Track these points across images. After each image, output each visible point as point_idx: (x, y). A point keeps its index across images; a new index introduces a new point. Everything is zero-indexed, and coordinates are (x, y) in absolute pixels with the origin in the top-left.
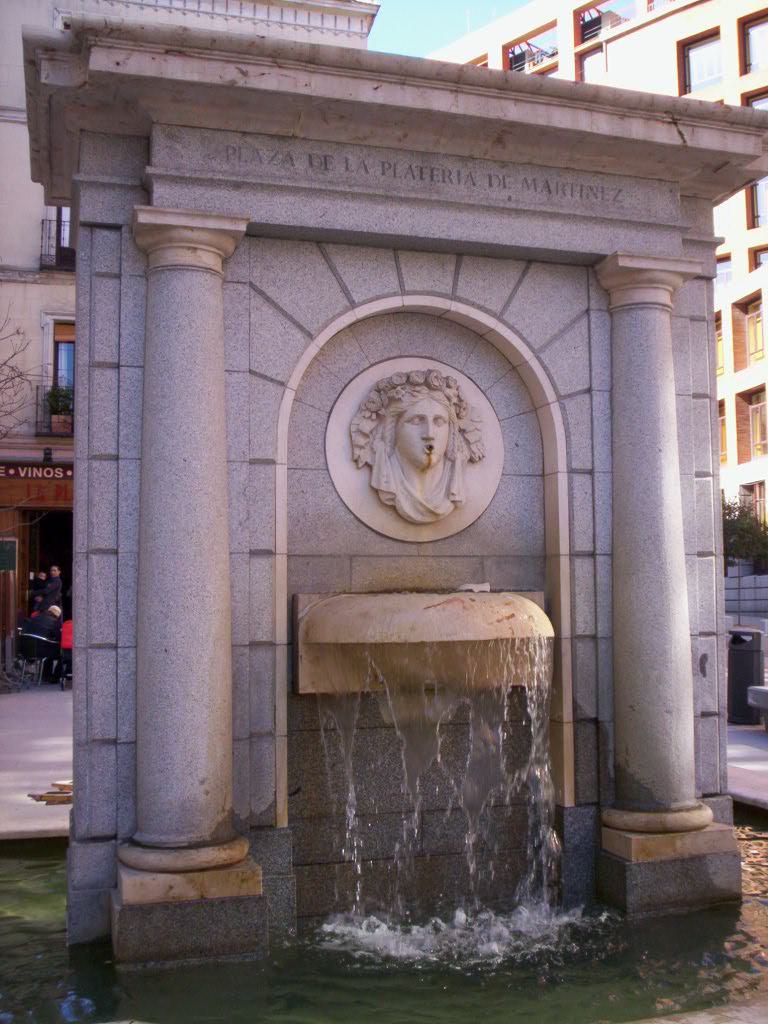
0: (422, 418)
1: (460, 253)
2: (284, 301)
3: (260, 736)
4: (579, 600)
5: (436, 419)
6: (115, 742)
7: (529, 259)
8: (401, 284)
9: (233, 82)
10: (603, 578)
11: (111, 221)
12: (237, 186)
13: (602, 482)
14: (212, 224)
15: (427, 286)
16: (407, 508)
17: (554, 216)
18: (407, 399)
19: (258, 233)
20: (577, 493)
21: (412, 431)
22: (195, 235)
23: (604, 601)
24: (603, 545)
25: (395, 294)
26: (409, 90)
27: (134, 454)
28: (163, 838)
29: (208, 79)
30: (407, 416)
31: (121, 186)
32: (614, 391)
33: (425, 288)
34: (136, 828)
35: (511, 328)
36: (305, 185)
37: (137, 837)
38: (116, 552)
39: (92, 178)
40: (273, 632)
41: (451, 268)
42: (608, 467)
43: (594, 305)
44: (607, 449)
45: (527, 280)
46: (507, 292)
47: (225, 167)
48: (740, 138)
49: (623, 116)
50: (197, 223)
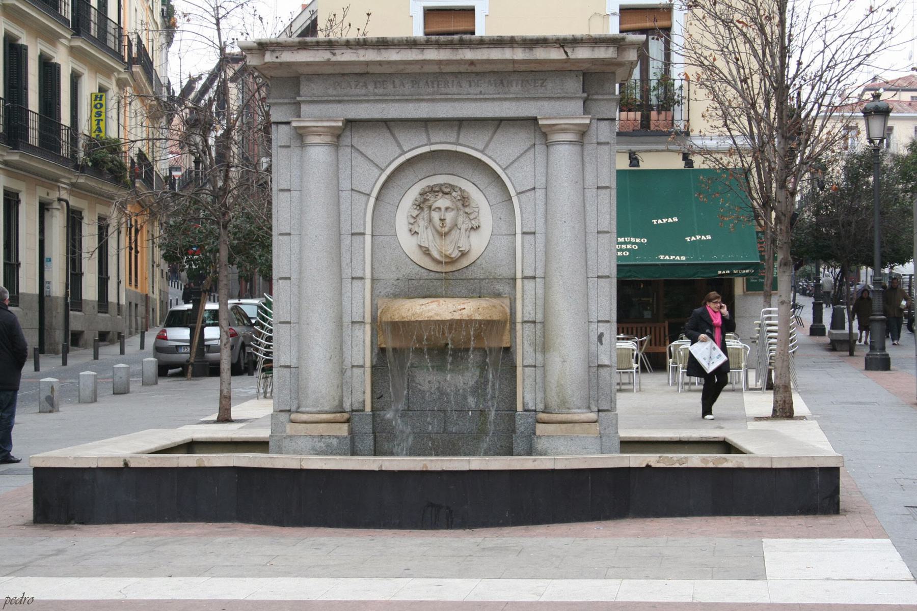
0: (440, 209)
1: (460, 124)
2: (369, 153)
3: (460, 350)
4: (527, 301)
5: (447, 209)
6: (534, 322)
7: (499, 123)
8: (429, 139)
9: (329, 60)
10: (540, 292)
11: (285, 120)
12: (340, 102)
13: (540, 238)
14: (325, 124)
15: (443, 140)
16: (436, 254)
17: (506, 99)
18: (432, 199)
19: (351, 124)
20: (527, 246)
21: (436, 216)
22: (319, 129)
23: (540, 303)
24: (540, 273)
25: (426, 145)
26: (414, 51)
27: (297, 232)
28: (307, 409)
29: (317, 59)
30: (433, 207)
31: (289, 103)
32: (549, 189)
33: (442, 142)
34: (546, 407)
35: (490, 157)
36: (372, 98)
37: (300, 410)
38: (290, 279)
39: (276, 101)
40: (364, 317)
41: (456, 128)
42: (544, 231)
43: (538, 142)
44: (543, 220)
45: (496, 137)
46: (487, 138)
47: (334, 93)
48: (602, 50)
49: (531, 49)
50: (319, 124)
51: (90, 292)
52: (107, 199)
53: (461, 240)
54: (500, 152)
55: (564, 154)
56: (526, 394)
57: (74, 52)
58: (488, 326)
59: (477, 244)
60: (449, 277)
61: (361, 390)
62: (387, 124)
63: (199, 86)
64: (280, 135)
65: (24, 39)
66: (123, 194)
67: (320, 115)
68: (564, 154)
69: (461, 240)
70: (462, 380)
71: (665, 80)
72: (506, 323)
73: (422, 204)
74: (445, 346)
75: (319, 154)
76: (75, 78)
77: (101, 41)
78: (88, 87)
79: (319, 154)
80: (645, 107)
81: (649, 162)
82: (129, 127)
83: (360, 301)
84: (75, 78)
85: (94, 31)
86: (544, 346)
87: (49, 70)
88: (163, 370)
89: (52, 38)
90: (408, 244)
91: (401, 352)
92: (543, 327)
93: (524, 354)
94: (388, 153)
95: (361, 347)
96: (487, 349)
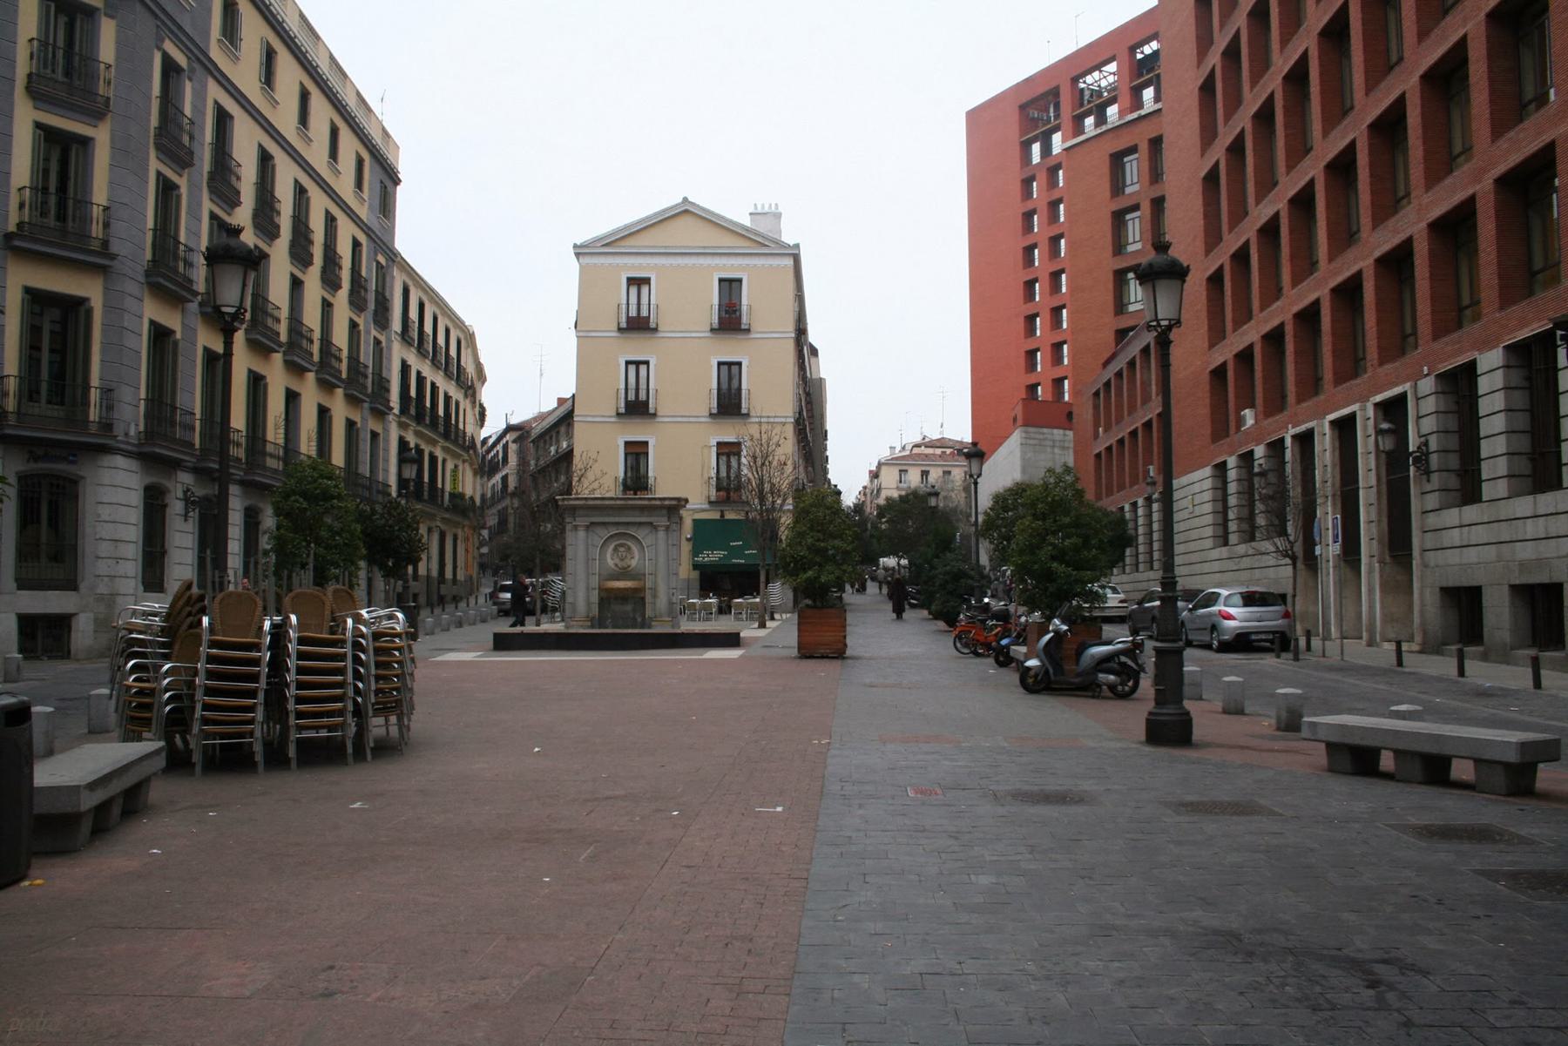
1: (628, 524)
7: (640, 524)
51: (449, 574)
52: (457, 525)
53: (628, 562)
54: (640, 534)
55: (661, 534)
56: (649, 613)
57: (445, 449)
58: (636, 590)
59: (634, 563)
60: (624, 573)
61: (595, 611)
62: (604, 524)
63: (491, 441)
64: (568, 527)
65: (423, 446)
66: (466, 523)
67: (582, 521)
68: (661, 534)
69: (628, 562)
70: (629, 608)
71: (739, 475)
72: (641, 590)
73: (615, 549)
74: (623, 596)
75: (581, 534)
76: (444, 461)
77: (455, 442)
78: (450, 466)
79: (581, 534)
80: (728, 490)
81: (730, 516)
82: (470, 486)
83: (595, 582)
84: (444, 461)
85: (441, 429)
86: (655, 596)
87: (433, 459)
88: (90, 732)
89: (433, 443)
90: (610, 562)
91: (608, 598)
92: (654, 590)
93: (648, 599)
94: (605, 533)
95: (595, 597)
96: (636, 598)
